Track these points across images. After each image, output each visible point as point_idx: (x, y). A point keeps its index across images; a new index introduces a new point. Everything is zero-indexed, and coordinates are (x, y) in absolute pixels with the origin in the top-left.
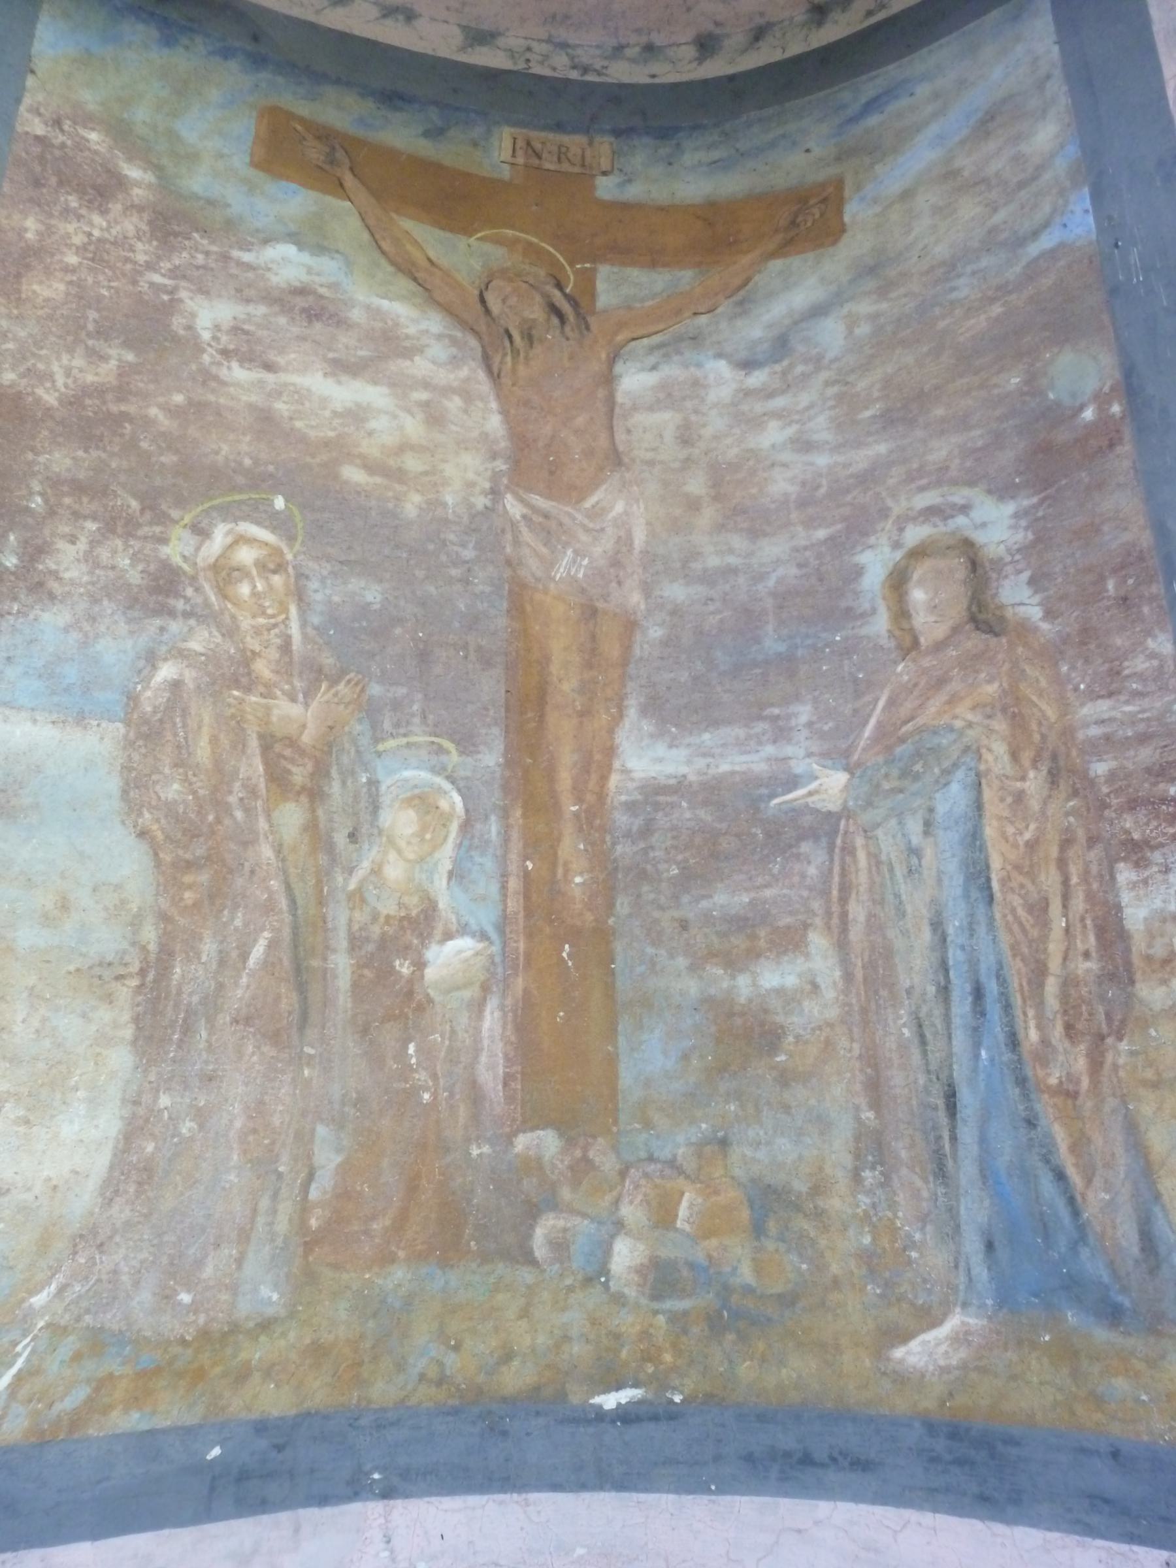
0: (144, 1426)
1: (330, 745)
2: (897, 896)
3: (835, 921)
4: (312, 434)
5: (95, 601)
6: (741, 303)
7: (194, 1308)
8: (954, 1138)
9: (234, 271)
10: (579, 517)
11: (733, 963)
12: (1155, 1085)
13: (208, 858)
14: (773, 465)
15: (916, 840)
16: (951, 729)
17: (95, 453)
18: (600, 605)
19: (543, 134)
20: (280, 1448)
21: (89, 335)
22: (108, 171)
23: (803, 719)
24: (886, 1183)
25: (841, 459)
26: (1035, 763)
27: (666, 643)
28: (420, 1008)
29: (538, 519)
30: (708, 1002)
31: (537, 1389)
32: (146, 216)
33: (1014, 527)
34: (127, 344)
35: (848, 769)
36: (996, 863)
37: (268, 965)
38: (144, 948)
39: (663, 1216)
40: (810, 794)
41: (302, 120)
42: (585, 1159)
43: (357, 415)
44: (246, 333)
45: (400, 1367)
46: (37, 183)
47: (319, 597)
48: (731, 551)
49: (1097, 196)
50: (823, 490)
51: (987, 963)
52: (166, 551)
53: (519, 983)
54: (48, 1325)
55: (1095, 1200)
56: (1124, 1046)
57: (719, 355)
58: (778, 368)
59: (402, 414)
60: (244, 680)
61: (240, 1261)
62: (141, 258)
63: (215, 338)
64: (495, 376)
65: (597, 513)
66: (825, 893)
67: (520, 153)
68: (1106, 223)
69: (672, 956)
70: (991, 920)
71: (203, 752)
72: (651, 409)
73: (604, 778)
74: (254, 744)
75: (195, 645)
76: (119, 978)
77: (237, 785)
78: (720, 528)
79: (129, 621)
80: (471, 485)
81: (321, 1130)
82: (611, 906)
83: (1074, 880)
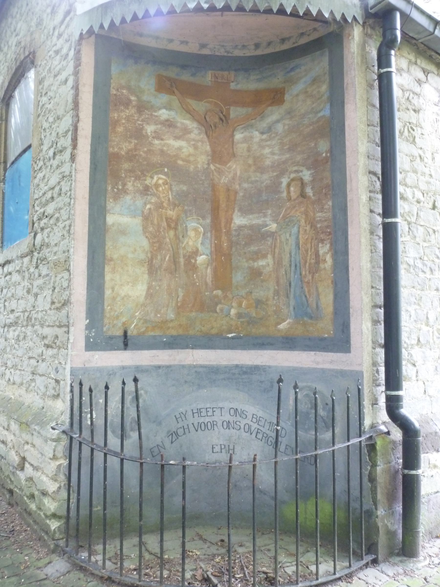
0: (154, 335)
1: (178, 219)
2: (284, 248)
3: (273, 253)
4: (171, 154)
5: (135, 194)
6: (262, 117)
7: (160, 317)
8: (290, 291)
9: (154, 118)
10: (226, 169)
11: (254, 260)
12: (321, 281)
13: (158, 241)
14: (266, 158)
15: (288, 237)
16: (295, 216)
17: (132, 163)
18: (230, 188)
19: (218, 72)
20: (175, 340)
21: (129, 138)
22: (128, 99)
23: (269, 213)
24: (278, 299)
25: (280, 157)
26: (309, 223)
27: (243, 196)
28: (196, 268)
29: (217, 170)
30: (249, 268)
31: (218, 333)
32: (136, 108)
33: (310, 177)
34: (135, 139)
35: (277, 223)
36: (301, 242)
37: (169, 260)
38: (148, 257)
39: (240, 305)
40: (270, 228)
41: (166, 77)
42: (226, 295)
43: (180, 148)
44: (157, 132)
45: (194, 329)
46: (116, 105)
47: (174, 189)
48: (257, 177)
49: (331, 105)
50: (276, 164)
51: (298, 260)
52: (146, 182)
53: (214, 264)
54: (139, 318)
55: (311, 300)
56: (317, 275)
57: (257, 130)
58: (269, 134)
59: (189, 147)
60: (162, 207)
61: (167, 310)
62: (136, 118)
63: (151, 134)
64: (208, 137)
65: (230, 168)
66: (271, 247)
67: (213, 78)
68: (332, 112)
69: (243, 259)
70: (299, 253)
71: (155, 222)
72: (241, 143)
73: (230, 224)
74: (164, 219)
75: (153, 201)
76: (145, 263)
77: (162, 228)
78: (255, 171)
79: (141, 197)
80: (203, 163)
81: (180, 289)
82: (231, 249)
83: (313, 246)
